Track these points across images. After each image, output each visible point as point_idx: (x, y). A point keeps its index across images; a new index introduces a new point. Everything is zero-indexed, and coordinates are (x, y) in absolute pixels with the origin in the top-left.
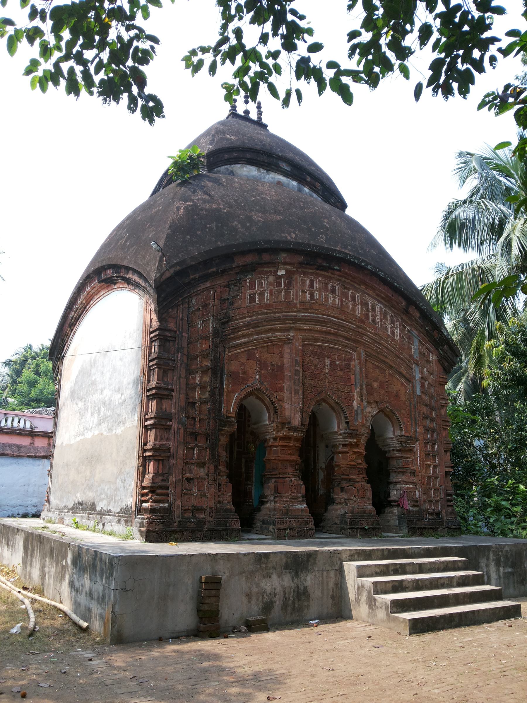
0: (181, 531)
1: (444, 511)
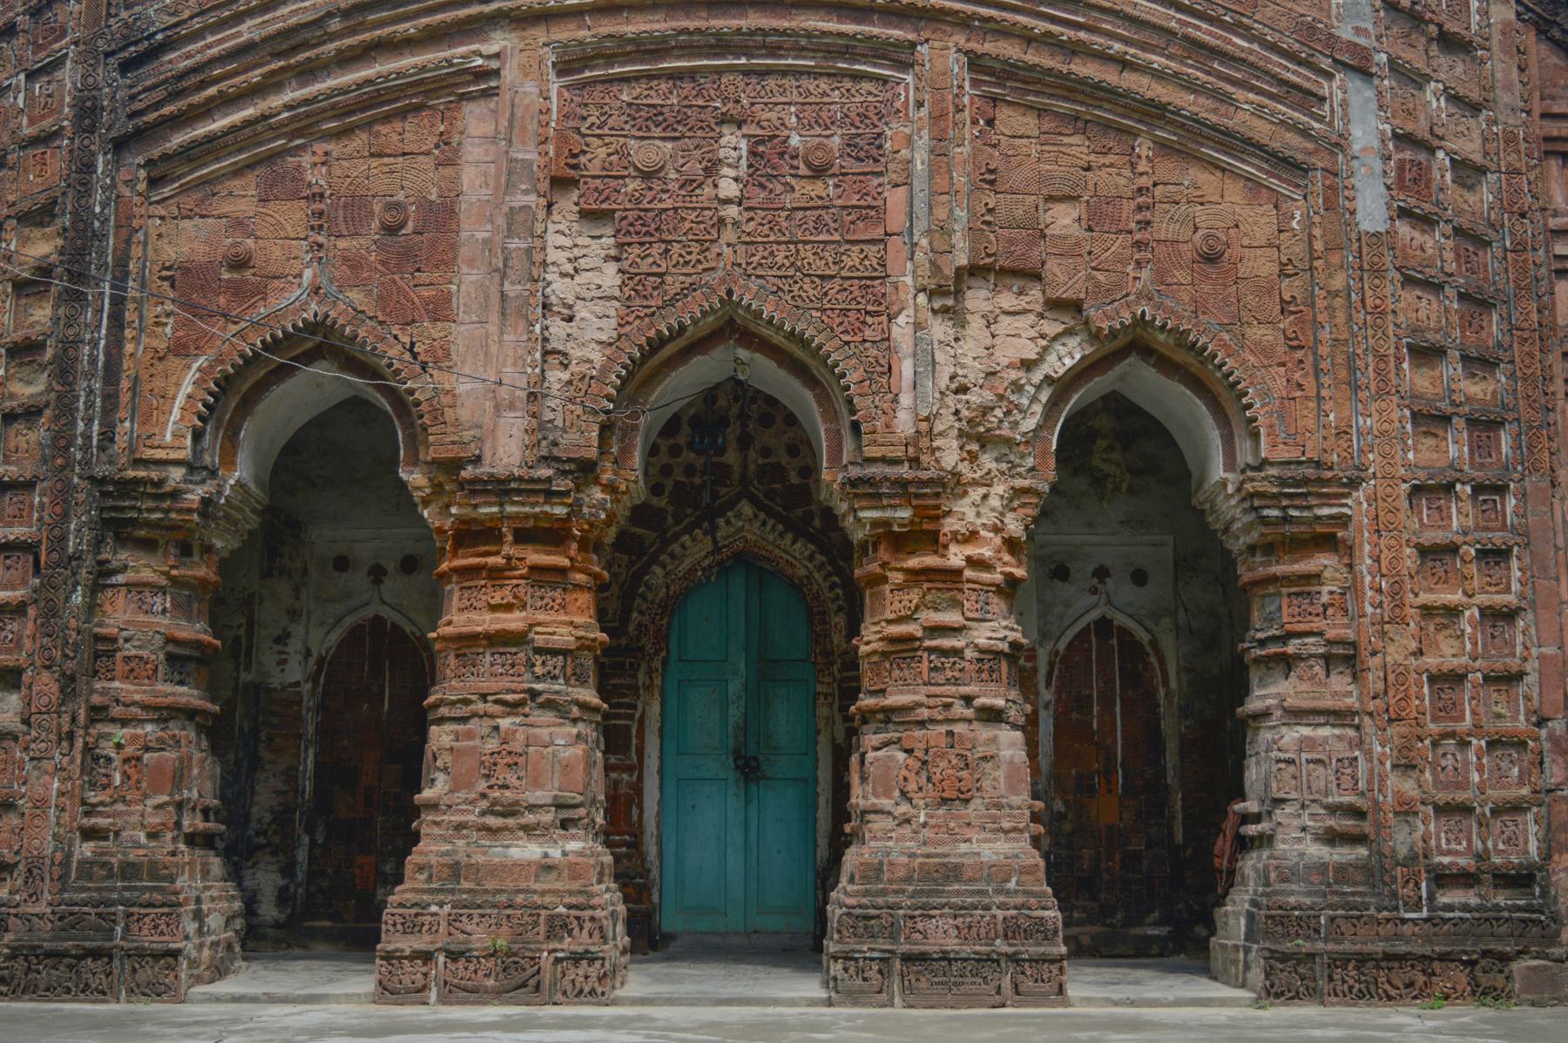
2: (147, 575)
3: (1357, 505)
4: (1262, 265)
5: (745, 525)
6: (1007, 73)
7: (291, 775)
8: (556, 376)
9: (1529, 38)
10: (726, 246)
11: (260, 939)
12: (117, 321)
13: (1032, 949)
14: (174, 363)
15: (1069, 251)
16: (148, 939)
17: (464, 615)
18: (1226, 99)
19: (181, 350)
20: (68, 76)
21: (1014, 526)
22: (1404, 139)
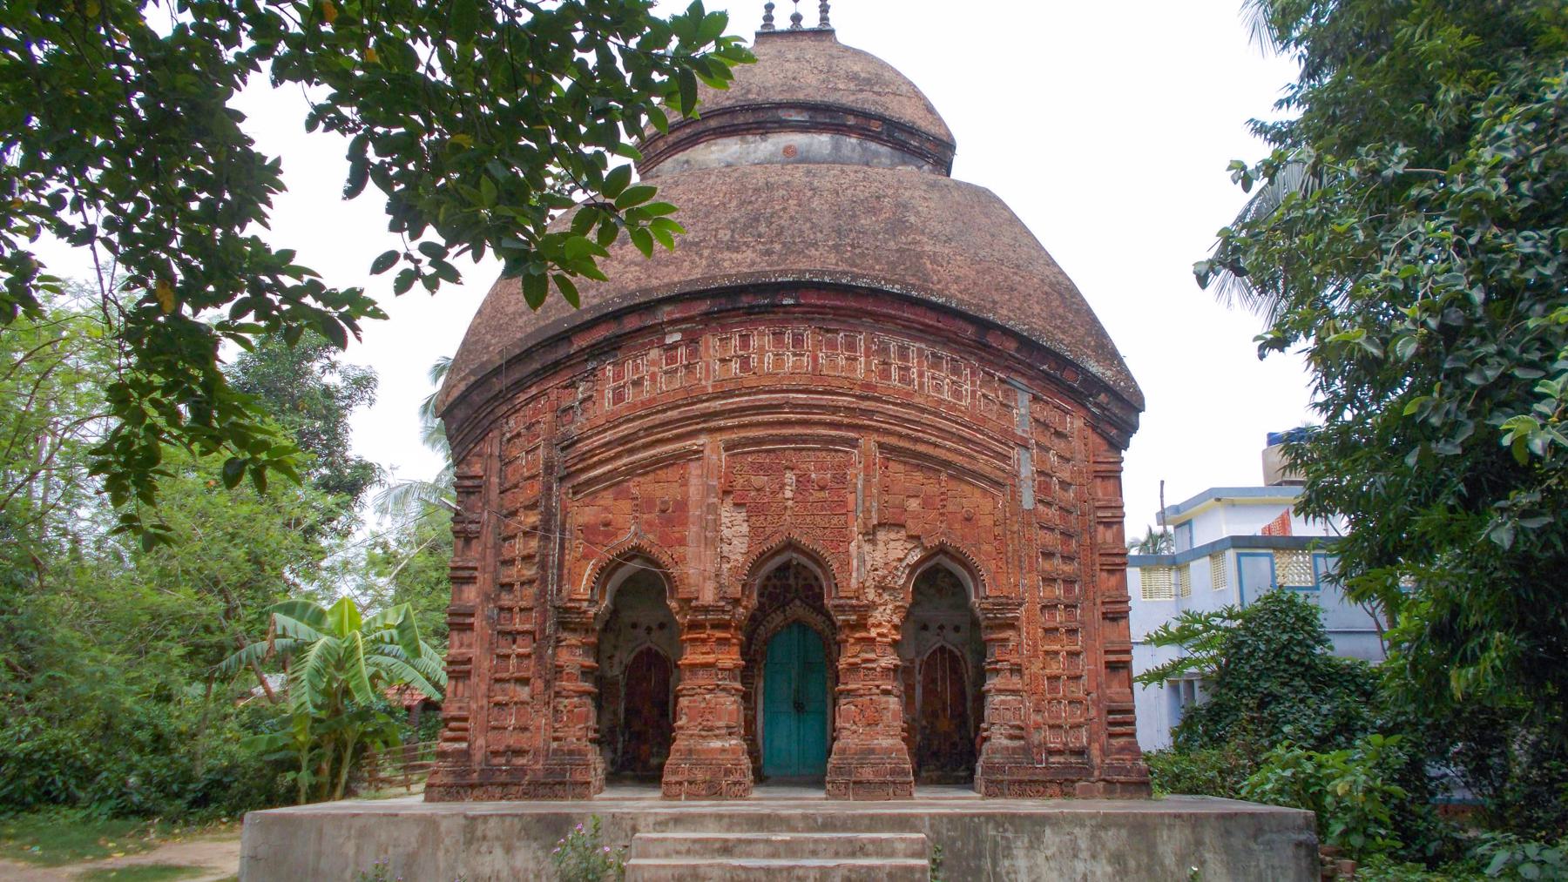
0: (481, 785)
1: (1096, 746)
2: (574, 642)
3: (1021, 612)
4: (987, 521)
5: (798, 609)
6: (893, 449)
7: (615, 713)
8: (726, 566)
9: (1089, 432)
10: (787, 517)
11: (615, 777)
12: (562, 547)
13: (899, 779)
14: (583, 562)
15: (916, 516)
16: (579, 778)
17: (691, 656)
18: (974, 458)
19: (586, 557)
20: (541, 452)
21: (896, 620)
22: (1041, 473)
